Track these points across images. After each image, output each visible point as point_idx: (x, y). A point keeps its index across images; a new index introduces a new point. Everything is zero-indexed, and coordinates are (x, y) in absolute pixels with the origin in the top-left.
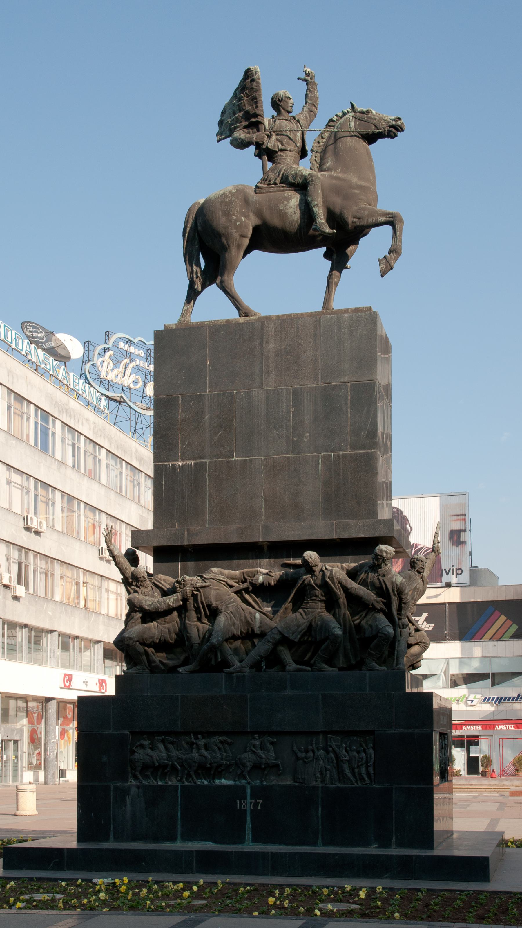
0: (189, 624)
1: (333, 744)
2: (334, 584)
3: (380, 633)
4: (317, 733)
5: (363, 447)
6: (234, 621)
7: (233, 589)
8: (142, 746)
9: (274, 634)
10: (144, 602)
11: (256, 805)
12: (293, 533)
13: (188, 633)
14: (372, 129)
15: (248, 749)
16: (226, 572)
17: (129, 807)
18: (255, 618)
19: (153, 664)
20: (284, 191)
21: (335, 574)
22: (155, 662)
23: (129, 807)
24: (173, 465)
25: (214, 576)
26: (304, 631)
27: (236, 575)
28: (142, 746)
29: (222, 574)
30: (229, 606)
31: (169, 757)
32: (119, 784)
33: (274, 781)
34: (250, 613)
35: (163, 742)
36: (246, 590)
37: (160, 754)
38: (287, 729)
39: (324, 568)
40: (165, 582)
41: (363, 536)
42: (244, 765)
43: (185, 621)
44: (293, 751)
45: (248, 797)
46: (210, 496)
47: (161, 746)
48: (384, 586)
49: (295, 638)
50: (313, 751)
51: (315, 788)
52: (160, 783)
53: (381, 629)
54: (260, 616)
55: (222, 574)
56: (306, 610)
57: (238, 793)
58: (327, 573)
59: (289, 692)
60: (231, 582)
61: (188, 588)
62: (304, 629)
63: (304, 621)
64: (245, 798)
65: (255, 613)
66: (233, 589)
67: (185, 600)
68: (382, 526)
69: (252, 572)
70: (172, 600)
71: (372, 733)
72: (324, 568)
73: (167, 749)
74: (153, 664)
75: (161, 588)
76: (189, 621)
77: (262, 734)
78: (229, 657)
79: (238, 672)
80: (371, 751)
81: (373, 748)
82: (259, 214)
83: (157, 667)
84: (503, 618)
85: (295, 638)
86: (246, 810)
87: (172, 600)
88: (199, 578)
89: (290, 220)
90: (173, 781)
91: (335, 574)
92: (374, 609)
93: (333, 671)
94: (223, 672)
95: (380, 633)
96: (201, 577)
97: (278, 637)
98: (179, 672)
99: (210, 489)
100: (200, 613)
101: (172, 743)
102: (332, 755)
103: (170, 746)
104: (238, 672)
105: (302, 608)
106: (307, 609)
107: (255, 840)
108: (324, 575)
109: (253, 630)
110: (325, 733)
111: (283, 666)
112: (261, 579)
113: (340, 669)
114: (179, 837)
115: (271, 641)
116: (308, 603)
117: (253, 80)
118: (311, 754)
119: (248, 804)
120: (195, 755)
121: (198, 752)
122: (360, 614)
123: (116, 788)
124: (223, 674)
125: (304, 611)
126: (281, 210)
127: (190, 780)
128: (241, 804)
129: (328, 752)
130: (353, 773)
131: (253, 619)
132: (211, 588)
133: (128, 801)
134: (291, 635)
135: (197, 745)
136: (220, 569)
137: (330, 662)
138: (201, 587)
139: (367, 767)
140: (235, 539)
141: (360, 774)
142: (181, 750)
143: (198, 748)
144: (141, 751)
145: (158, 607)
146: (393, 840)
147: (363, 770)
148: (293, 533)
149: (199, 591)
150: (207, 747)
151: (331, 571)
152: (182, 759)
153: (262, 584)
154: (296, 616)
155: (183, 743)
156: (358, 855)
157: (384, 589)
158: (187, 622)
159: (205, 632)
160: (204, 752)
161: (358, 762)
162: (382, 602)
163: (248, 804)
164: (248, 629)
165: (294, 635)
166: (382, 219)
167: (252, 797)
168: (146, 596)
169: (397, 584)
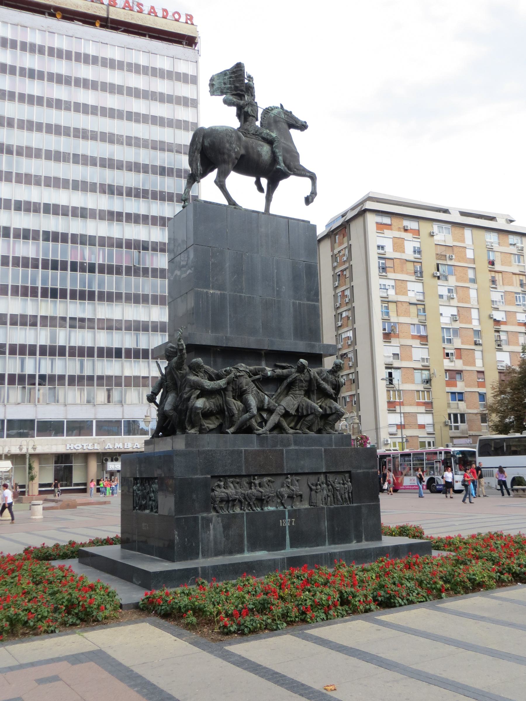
1: (330, 480)
4: (320, 473)
5: (312, 301)
8: (219, 486)
11: (291, 522)
14: (292, 122)
15: (285, 485)
20: (259, 140)
22: (204, 426)
23: (212, 532)
24: (207, 292)
28: (219, 486)
29: (246, 368)
31: (237, 492)
32: (205, 515)
34: (262, 395)
35: (232, 483)
36: (258, 379)
37: (231, 491)
38: (307, 471)
42: (283, 496)
43: (225, 398)
44: (308, 485)
45: (287, 517)
46: (230, 315)
47: (231, 485)
50: (320, 485)
52: (231, 512)
55: (246, 368)
57: (281, 515)
59: (292, 447)
64: (285, 519)
67: (228, 383)
70: (222, 383)
71: (349, 472)
73: (235, 487)
77: (292, 474)
79: (264, 433)
80: (350, 484)
81: (351, 482)
82: (246, 148)
86: (285, 527)
89: (263, 158)
90: (238, 510)
93: (312, 434)
94: (255, 433)
96: (334, 375)
98: (227, 433)
99: (230, 311)
101: (238, 483)
102: (330, 487)
103: (236, 485)
104: (264, 433)
107: (292, 546)
108: (310, 374)
109: (263, 406)
110: (325, 473)
114: (246, 549)
117: (241, 70)
118: (319, 487)
119: (286, 523)
120: (254, 490)
121: (255, 489)
123: (203, 518)
126: (259, 151)
127: (249, 508)
128: (283, 522)
129: (328, 485)
130: (341, 497)
133: (211, 527)
135: (254, 483)
137: (310, 428)
138: (239, 376)
139: (349, 493)
141: (345, 498)
142: (243, 487)
143: (255, 486)
144: (218, 489)
146: (363, 537)
150: (260, 485)
152: (244, 494)
155: (245, 483)
156: (373, 548)
160: (258, 488)
161: (344, 490)
163: (286, 523)
166: (308, 174)
167: (289, 518)
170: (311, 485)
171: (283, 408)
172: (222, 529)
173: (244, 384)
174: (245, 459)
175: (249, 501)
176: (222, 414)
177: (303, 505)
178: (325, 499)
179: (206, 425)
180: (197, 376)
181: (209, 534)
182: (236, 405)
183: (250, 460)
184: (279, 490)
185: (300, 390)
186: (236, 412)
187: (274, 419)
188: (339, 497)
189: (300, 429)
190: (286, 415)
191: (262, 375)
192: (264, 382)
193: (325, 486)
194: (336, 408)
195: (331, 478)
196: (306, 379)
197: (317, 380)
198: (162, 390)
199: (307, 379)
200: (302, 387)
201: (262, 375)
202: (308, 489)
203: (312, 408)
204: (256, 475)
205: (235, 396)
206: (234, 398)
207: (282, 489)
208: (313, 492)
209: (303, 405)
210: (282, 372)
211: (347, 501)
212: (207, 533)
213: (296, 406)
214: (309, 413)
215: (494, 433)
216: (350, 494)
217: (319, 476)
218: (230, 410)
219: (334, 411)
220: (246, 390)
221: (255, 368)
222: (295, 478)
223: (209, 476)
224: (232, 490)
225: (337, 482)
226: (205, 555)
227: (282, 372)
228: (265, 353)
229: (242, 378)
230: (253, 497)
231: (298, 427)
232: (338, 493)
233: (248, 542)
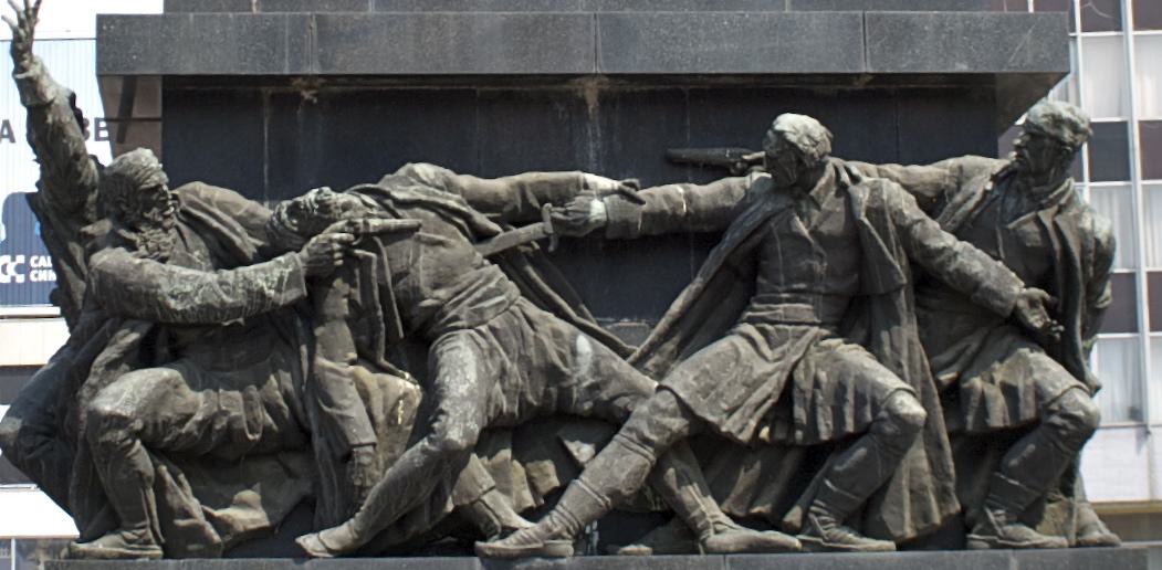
0: (332, 370)
2: (886, 239)
3: (1052, 412)
6: (503, 363)
7: (490, 247)
9: (664, 412)
10: (162, 281)
12: (714, 47)
13: (331, 404)
16: (465, 181)
18: (574, 353)
19: (181, 523)
21: (890, 197)
25: (427, 193)
26: (770, 402)
27: (496, 195)
29: (449, 186)
30: (486, 304)
34: (556, 334)
39: (845, 177)
40: (227, 211)
41: (962, 67)
48: (1057, 246)
49: (741, 431)
53: (1055, 400)
54: (594, 348)
55: (449, 186)
56: (769, 327)
58: (862, 195)
60: (481, 219)
61: (337, 236)
62: (769, 397)
63: (769, 367)
65: (575, 337)
66: (490, 247)
67: (317, 279)
68: (1028, 36)
69: (554, 185)
70: (271, 277)
72: (845, 177)
74: (181, 523)
75: (216, 232)
76: (330, 358)
78: (486, 498)
83: (196, 533)
84: (824, 437)
85: (741, 431)
87: (276, 273)
88: (369, 199)
91: (890, 197)
92: (1014, 327)
95: (1052, 412)
96: (381, 195)
97: (678, 424)
98: (302, 555)
100: (374, 330)
105: (751, 321)
106: (772, 323)
108: (849, 202)
109: (565, 394)
111: (689, 537)
112: (598, 209)
113: (903, 545)
115: (654, 438)
116: (780, 301)
122: (959, 347)
124: (477, 560)
125: (763, 332)
131: (569, 358)
132: (419, 239)
134: (725, 416)
136: (442, 170)
140: (498, 62)
145: (223, 303)
148: (714, 47)
149: (378, 252)
151: (875, 190)
153: (602, 229)
154: (737, 350)
157: (1058, 256)
158: (321, 361)
159: (391, 401)
162: (1043, 299)
164: (547, 394)
165: (736, 416)
168: (163, 260)
169: (1098, 242)
171: (673, 405)
173: (423, 278)
176: (304, 455)
180: (131, 246)
182: (364, 394)
185: (797, 296)
186: (362, 433)
187: (609, 468)
189: (805, 525)
190: (702, 445)
191: (555, 221)
192: (580, 265)
194: (1039, 393)
196: (824, 229)
197: (905, 232)
198: (530, 270)
199: (834, 226)
200: (809, 276)
201: (555, 221)
203: (871, 398)
205: (373, 345)
206: (366, 356)
209: (817, 384)
210: (689, 198)
213: (770, 387)
214: (850, 427)
218: (335, 427)
219: (1028, 413)
220: (438, 311)
221: (521, 186)
227: (689, 198)
228: (605, 100)
229: (407, 245)
231: (794, 516)
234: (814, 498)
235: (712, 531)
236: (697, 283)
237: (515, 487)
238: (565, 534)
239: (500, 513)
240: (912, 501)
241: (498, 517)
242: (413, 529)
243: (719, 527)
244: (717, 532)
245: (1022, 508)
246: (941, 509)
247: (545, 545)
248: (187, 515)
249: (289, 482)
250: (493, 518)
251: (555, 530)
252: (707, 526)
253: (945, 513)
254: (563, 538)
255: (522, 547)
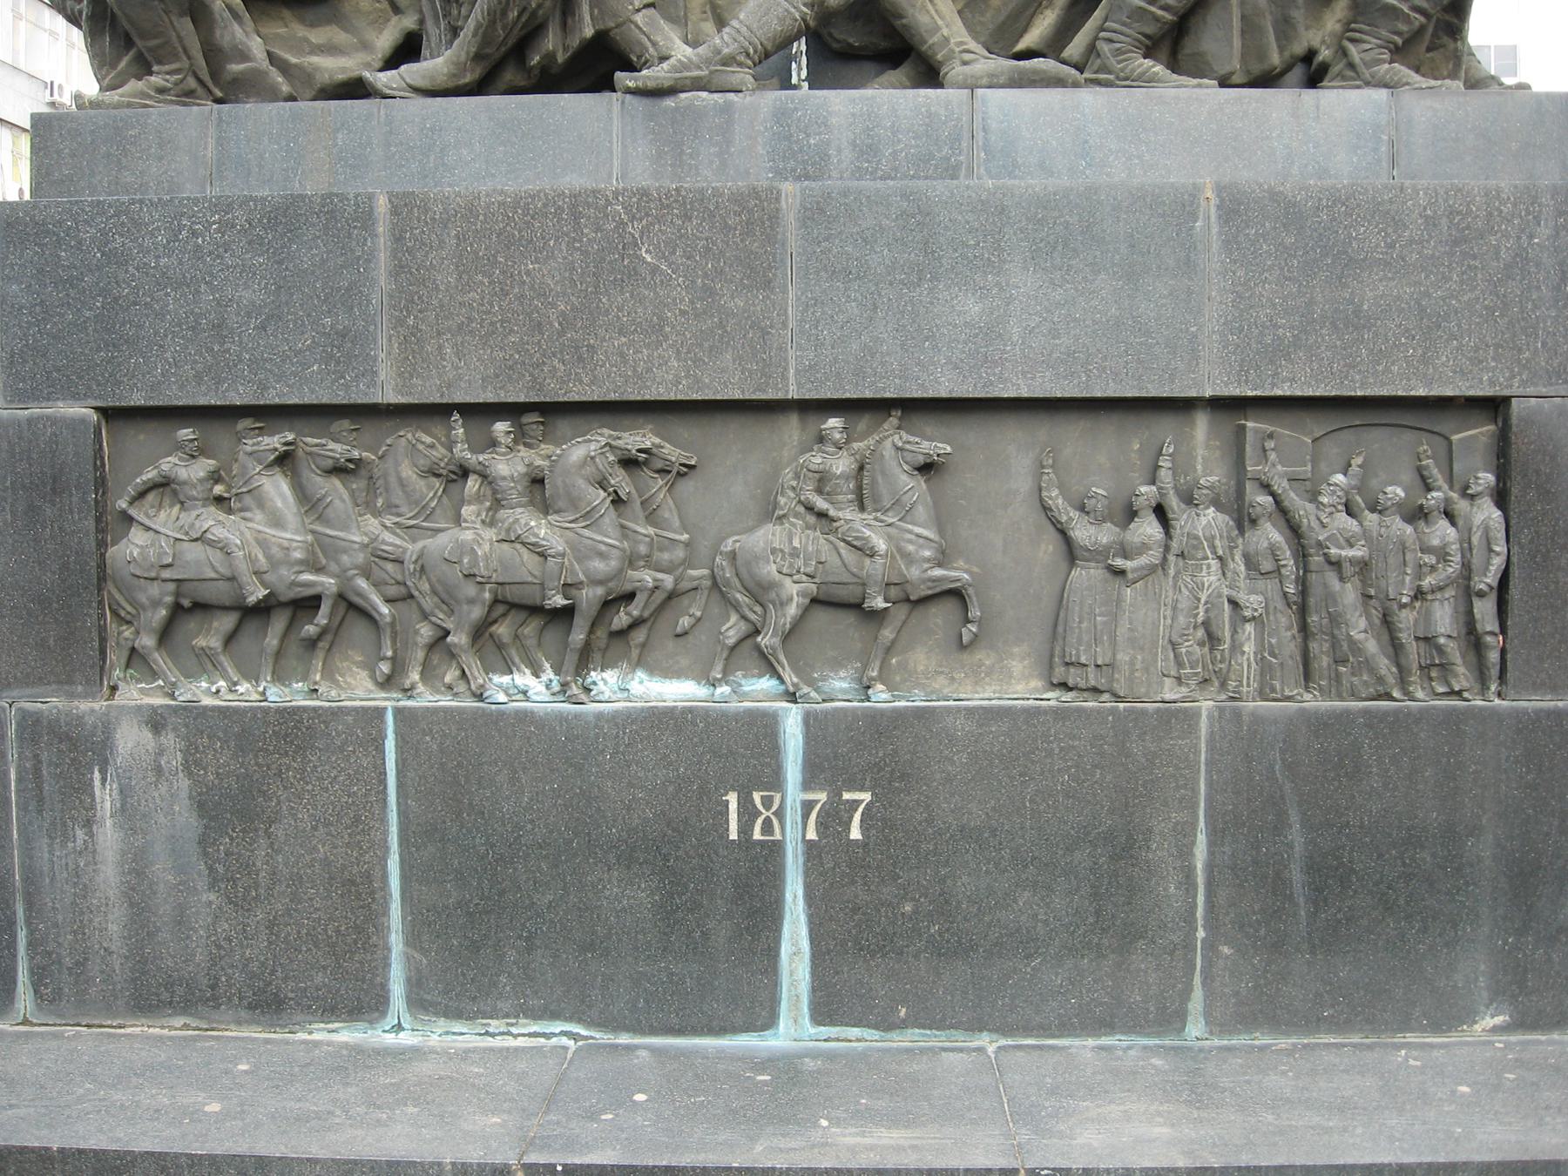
11: (834, 818)
17: (108, 835)
19: (236, 67)
23: (108, 835)
32: (53, 703)
33: (943, 686)
44: (1046, 509)
51: (1177, 719)
64: (775, 781)
71: (1494, 406)
73: (309, 502)
78: (638, 18)
80: (1487, 514)
81: (1501, 498)
86: (776, 849)
90: (355, 689)
102: (1271, 534)
103: (335, 491)
118: (1149, 528)
119: (793, 815)
128: (748, 813)
129: (1244, 520)
133: (105, 797)
139: (1469, 595)
142: (391, 508)
147: (1444, 619)
155: (407, 472)
170: (1068, 515)
172: (186, 818)
174: (398, 270)
175: (440, 616)
177: (978, 676)
178: (1212, 639)
179: (256, 46)
181: (90, 850)
183: (446, 278)
184: (728, 545)
188: (1359, 628)
193: (1210, 520)
195: (1279, 452)
202: (1049, 547)
204: (511, 411)
207: (768, 536)
208: (1086, 576)
211: (1445, 668)
212: (67, 837)
215: (1073, 1050)
216: (1485, 611)
217: (1164, 428)
222: (894, 443)
223: (82, 411)
224: (277, 522)
225: (1347, 499)
226: (57, 996)
230: (470, 590)
231: (1075, 48)
232: (1349, 594)
233: (1538, 712)
234: (1106, 20)
235: (958, 62)
236: (1198, 994)
237: (694, 17)
238: (742, 58)
239: (658, 39)
240: (1243, 32)
241: (654, 44)
242: (535, 60)
243: (967, 57)
244: (965, 63)
245: (1399, 41)
246: (1281, 49)
247: (712, 72)
248: (244, 56)
249: (395, 19)
250: (648, 44)
251: (726, 51)
252: (950, 56)
253: (1287, 54)
254: (740, 64)
255: (678, 75)
